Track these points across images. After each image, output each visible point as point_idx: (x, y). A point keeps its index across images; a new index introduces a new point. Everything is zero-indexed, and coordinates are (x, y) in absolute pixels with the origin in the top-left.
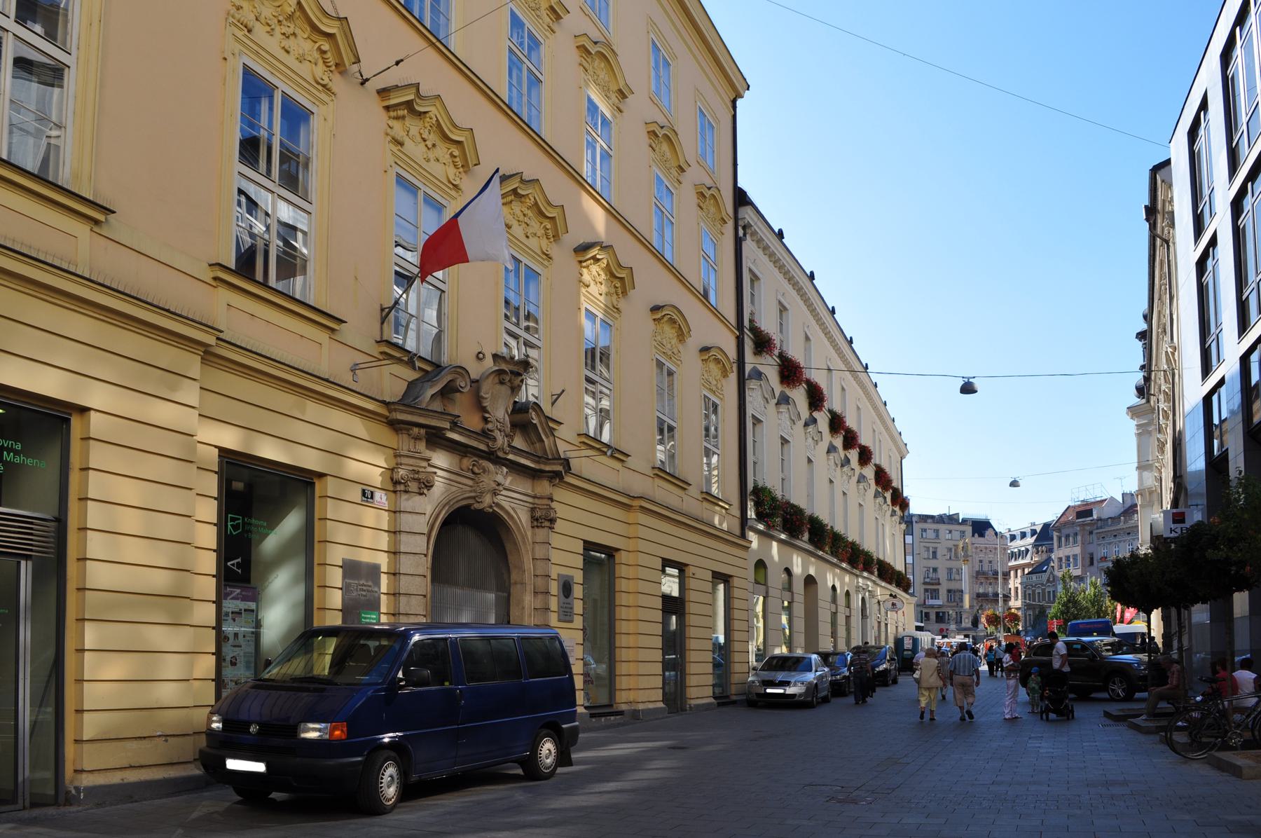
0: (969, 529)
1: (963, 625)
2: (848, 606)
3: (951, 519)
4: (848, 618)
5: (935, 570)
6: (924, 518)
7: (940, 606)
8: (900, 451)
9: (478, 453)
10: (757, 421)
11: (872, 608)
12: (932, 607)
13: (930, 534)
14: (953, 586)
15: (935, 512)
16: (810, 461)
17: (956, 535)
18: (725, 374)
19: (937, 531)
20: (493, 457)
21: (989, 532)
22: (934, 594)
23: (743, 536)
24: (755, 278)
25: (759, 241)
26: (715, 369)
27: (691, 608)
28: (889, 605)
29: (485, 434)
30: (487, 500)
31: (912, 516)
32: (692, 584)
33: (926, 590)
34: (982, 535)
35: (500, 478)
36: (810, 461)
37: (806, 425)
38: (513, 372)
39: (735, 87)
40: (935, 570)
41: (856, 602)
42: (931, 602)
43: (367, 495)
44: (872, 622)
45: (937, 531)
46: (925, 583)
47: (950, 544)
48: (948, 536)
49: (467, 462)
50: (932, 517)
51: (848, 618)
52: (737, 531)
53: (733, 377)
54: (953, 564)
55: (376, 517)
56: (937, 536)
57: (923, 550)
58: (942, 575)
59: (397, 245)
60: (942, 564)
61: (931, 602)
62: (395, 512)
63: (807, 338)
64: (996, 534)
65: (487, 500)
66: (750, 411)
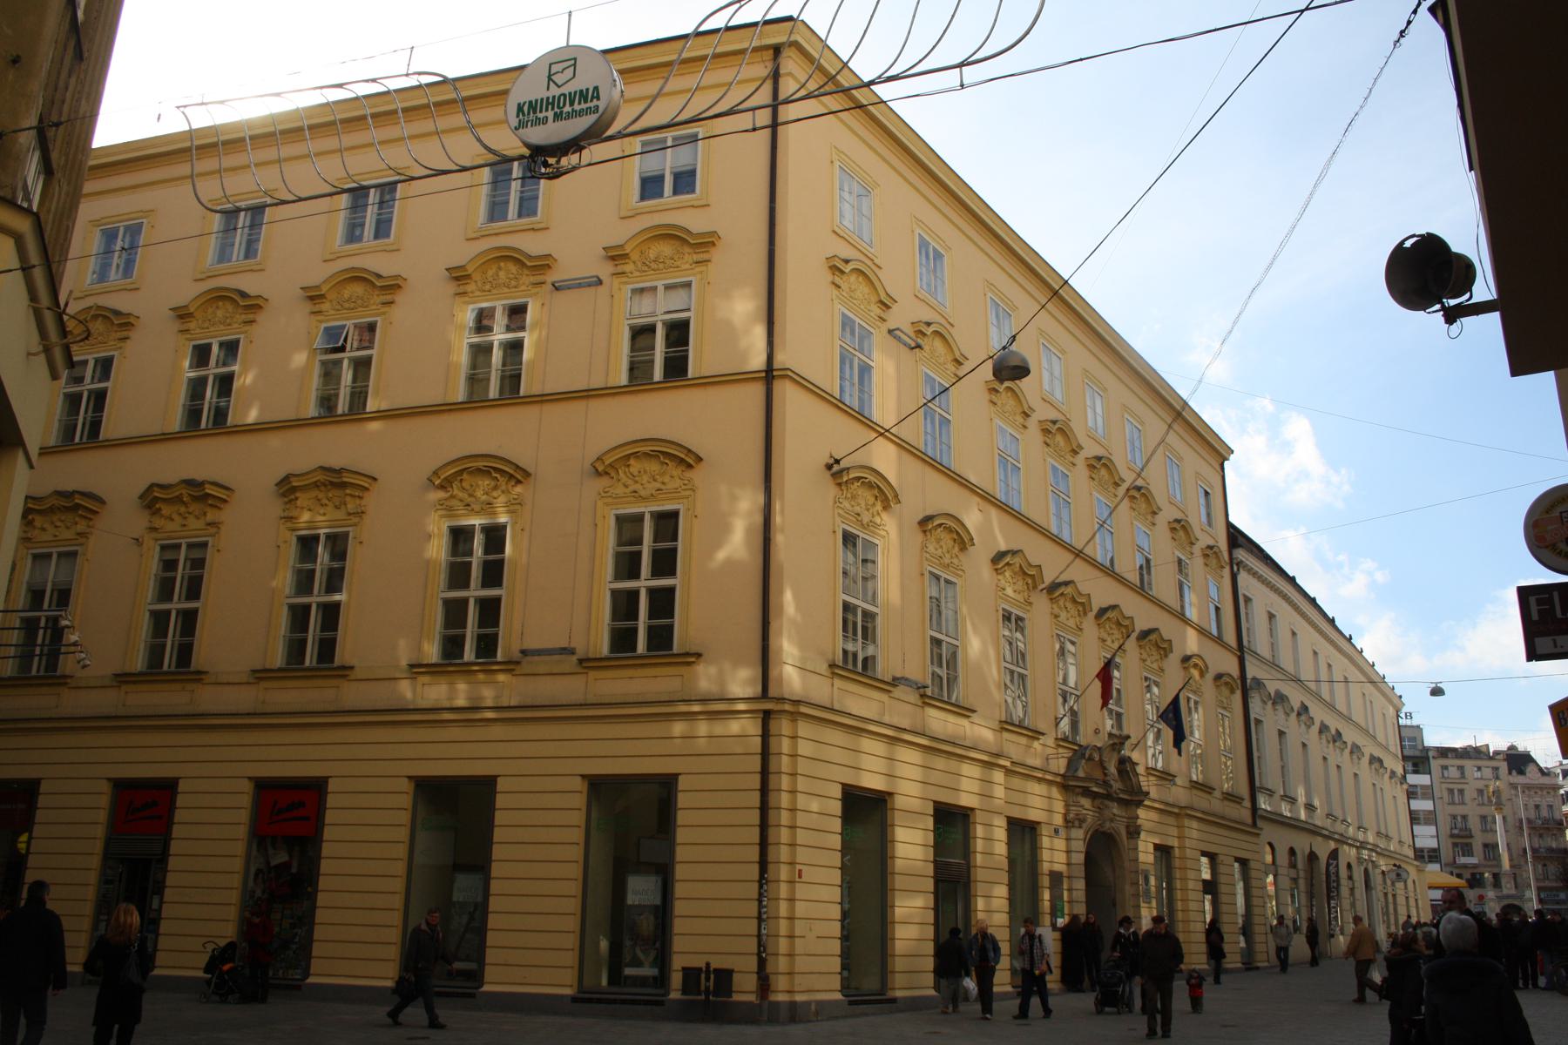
0: (1504, 766)
1: (1505, 892)
2: (1350, 878)
3: (1475, 753)
4: (1352, 890)
5: (1464, 817)
6: (1444, 752)
7: (1475, 866)
8: (1394, 706)
9: (1102, 798)
10: (1258, 722)
11: (1377, 879)
12: (1465, 866)
13: (1453, 773)
14: (1489, 839)
15: (1458, 744)
16: (1304, 745)
17: (1488, 773)
18: (1232, 691)
19: (1461, 768)
20: (1108, 797)
21: (1530, 768)
22: (1467, 850)
23: (1254, 824)
24: (1248, 600)
25: (1250, 571)
26: (1226, 691)
27: (1223, 889)
28: (1393, 876)
29: (1106, 784)
30: (1108, 825)
31: (1427, 749)
32: (1222, 869)
33: (1455, 845)
34: (1521, 772)
35: (1115, 811)
36: (1304, 745)
37: (1299, 714)
38: (1118, 741)
39: (1218, 453)
40: (1464, 817)
41: (1358, 875)
42: (1463, 860)
43: (1056, 831)
44: (1378, 893)
45: (1461, 768)
46: (1452, 836)
47: (1480, 784)
48: (1478, 775)
49: (1098, 802)
50: (1454, 750)
51: (1352, 890)
52: (1249, 821)
53: (1238, 693)
54: (1485, 810)
55: (1060, 844)
56: (1463, 775)
57: (1445, 794)
58: (1474, 824)
59: (1270, 844)
60: (1472, 811)
61: (1463, 860)
62: (1068, 839)
63: (1294, 634)
64: (1541, 769)
65: (1108, 825)
66: (1252, 716)
